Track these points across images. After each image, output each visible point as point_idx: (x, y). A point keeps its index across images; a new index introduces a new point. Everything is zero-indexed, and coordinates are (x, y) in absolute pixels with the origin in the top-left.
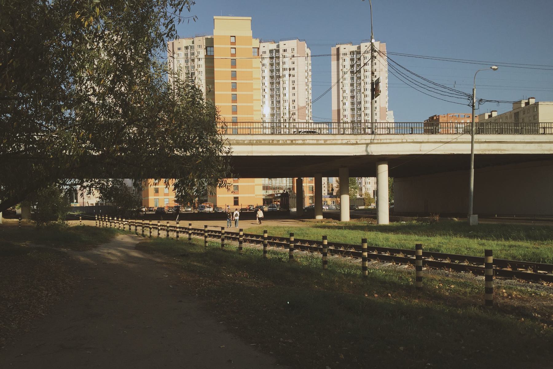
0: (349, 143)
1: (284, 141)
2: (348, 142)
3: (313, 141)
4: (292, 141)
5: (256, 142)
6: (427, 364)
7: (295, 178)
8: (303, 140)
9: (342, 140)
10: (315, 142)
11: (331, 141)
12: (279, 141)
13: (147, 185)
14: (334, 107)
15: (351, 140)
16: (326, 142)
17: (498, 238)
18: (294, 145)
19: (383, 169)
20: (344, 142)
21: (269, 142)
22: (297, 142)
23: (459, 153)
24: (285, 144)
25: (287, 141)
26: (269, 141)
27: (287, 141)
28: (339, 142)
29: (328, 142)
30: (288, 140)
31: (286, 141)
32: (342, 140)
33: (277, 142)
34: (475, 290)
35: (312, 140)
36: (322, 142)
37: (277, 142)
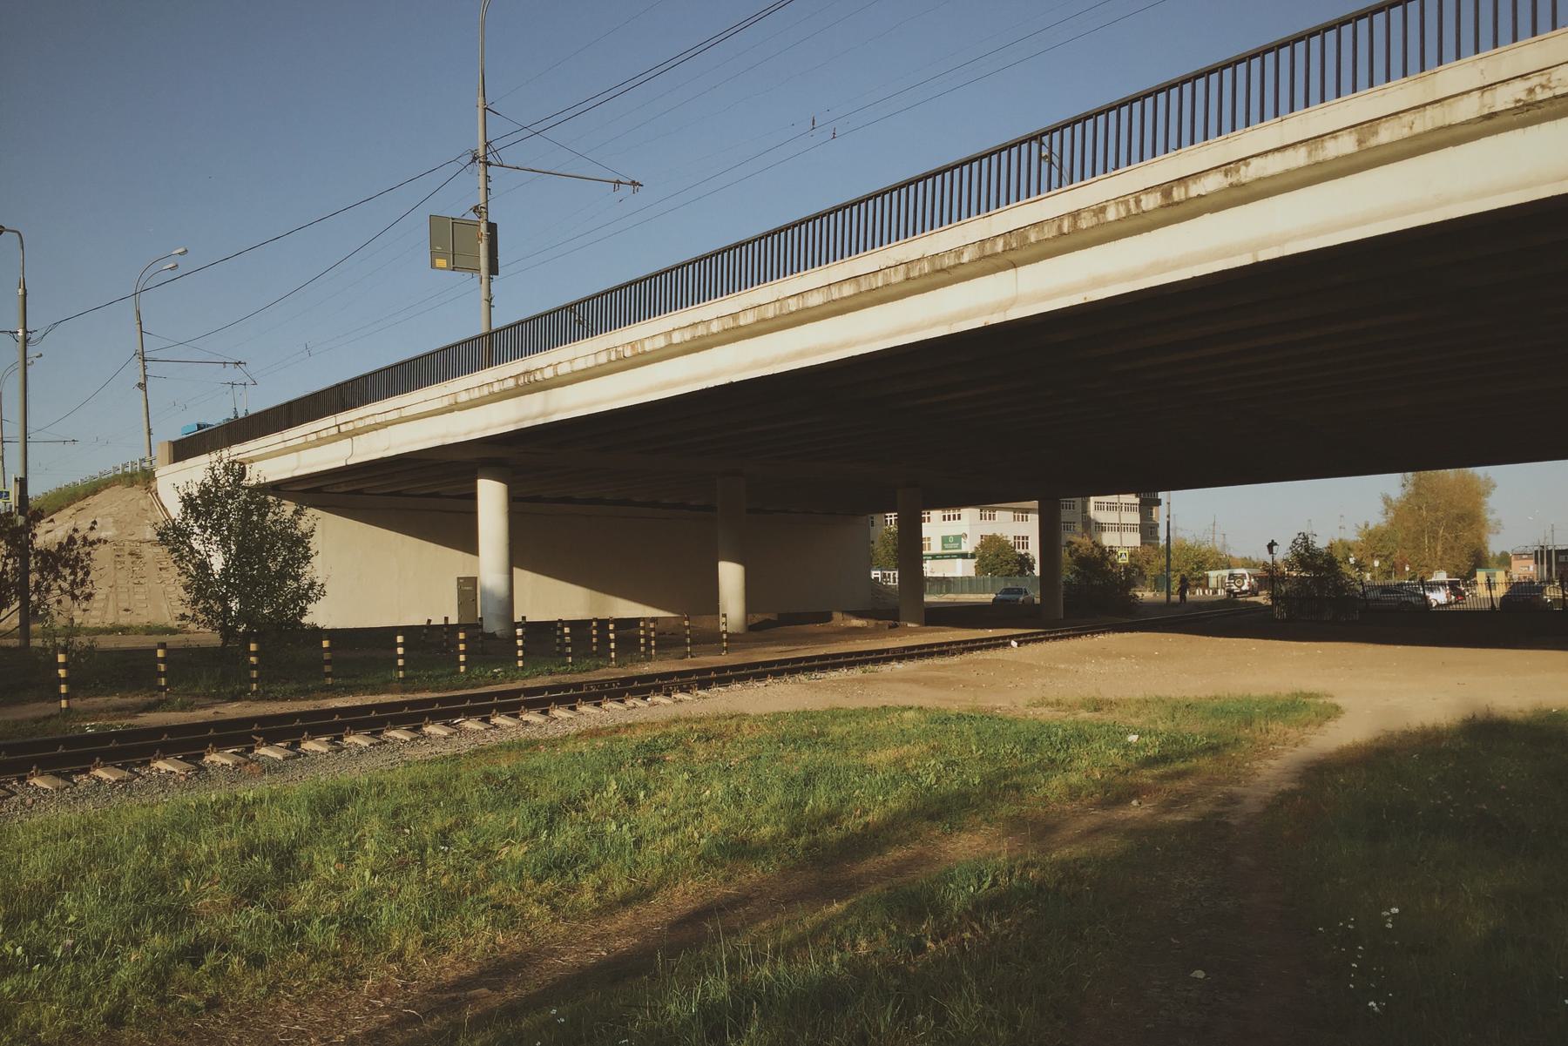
0: (1541, 95)
1: (1126, 203)
2: (1531, 91)
3: (1290, 153)
4: (1166, 189)
5: (1005, 244)
6: (1193, 975)
7: (1092, 498)
8: (1227, 168)
9: (1482, 89)
10: (1298, 158)
11: (1407, 118)
12: (1102, 210)
13: (1089, 501)
14: (14, 471)
15: (1557, 74)
16: (1373, 142)
17: (1142, 784)
18: (1207, 216)
19: (491, 496)
20: (1503, 99)
21: (1060, 227)
22: (1196, 189)
23: (283, 478)
24: (1136, 224)
25: (1143, 197)
26: (1057, 222)
27: (1143, 197)
28: (1468, 109)
29: (1386, 135)
30: (1146, 190)
31: (1138, 202)
32: (1487, 94)
33: (1094, 221)
34: (220, 621)
35: (1278, 155)
36: (1346, 145)
37: (1095, 220)
